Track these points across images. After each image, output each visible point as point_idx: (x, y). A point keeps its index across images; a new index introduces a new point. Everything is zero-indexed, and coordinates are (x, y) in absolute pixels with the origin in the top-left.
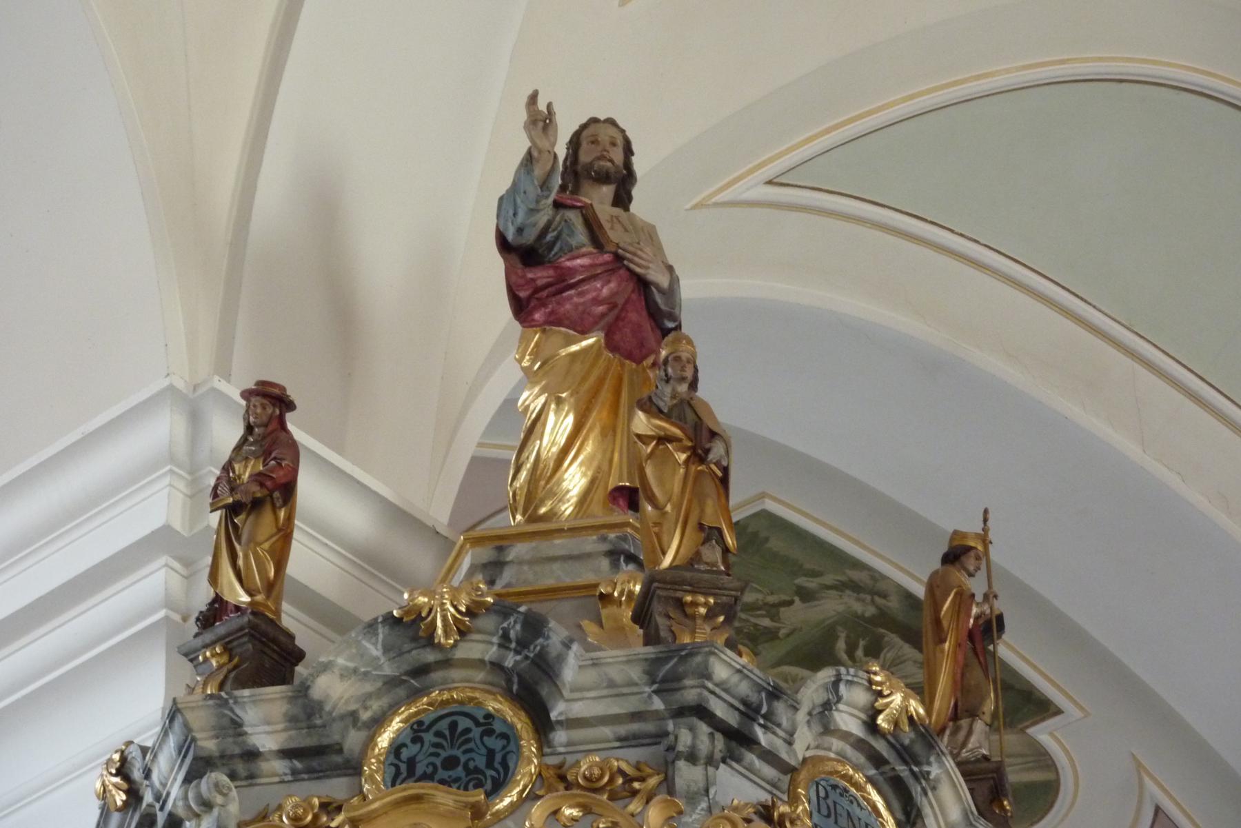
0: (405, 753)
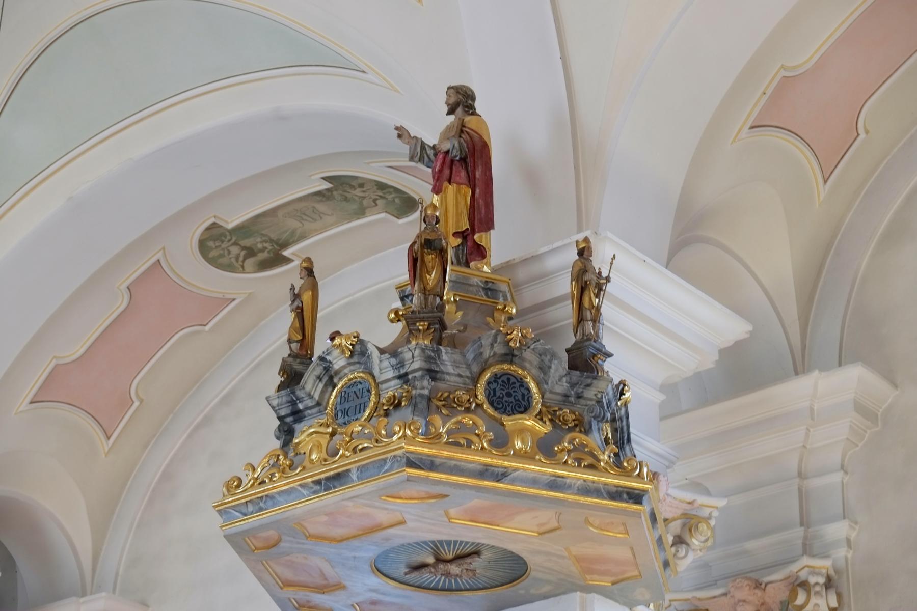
0: (494, 386)
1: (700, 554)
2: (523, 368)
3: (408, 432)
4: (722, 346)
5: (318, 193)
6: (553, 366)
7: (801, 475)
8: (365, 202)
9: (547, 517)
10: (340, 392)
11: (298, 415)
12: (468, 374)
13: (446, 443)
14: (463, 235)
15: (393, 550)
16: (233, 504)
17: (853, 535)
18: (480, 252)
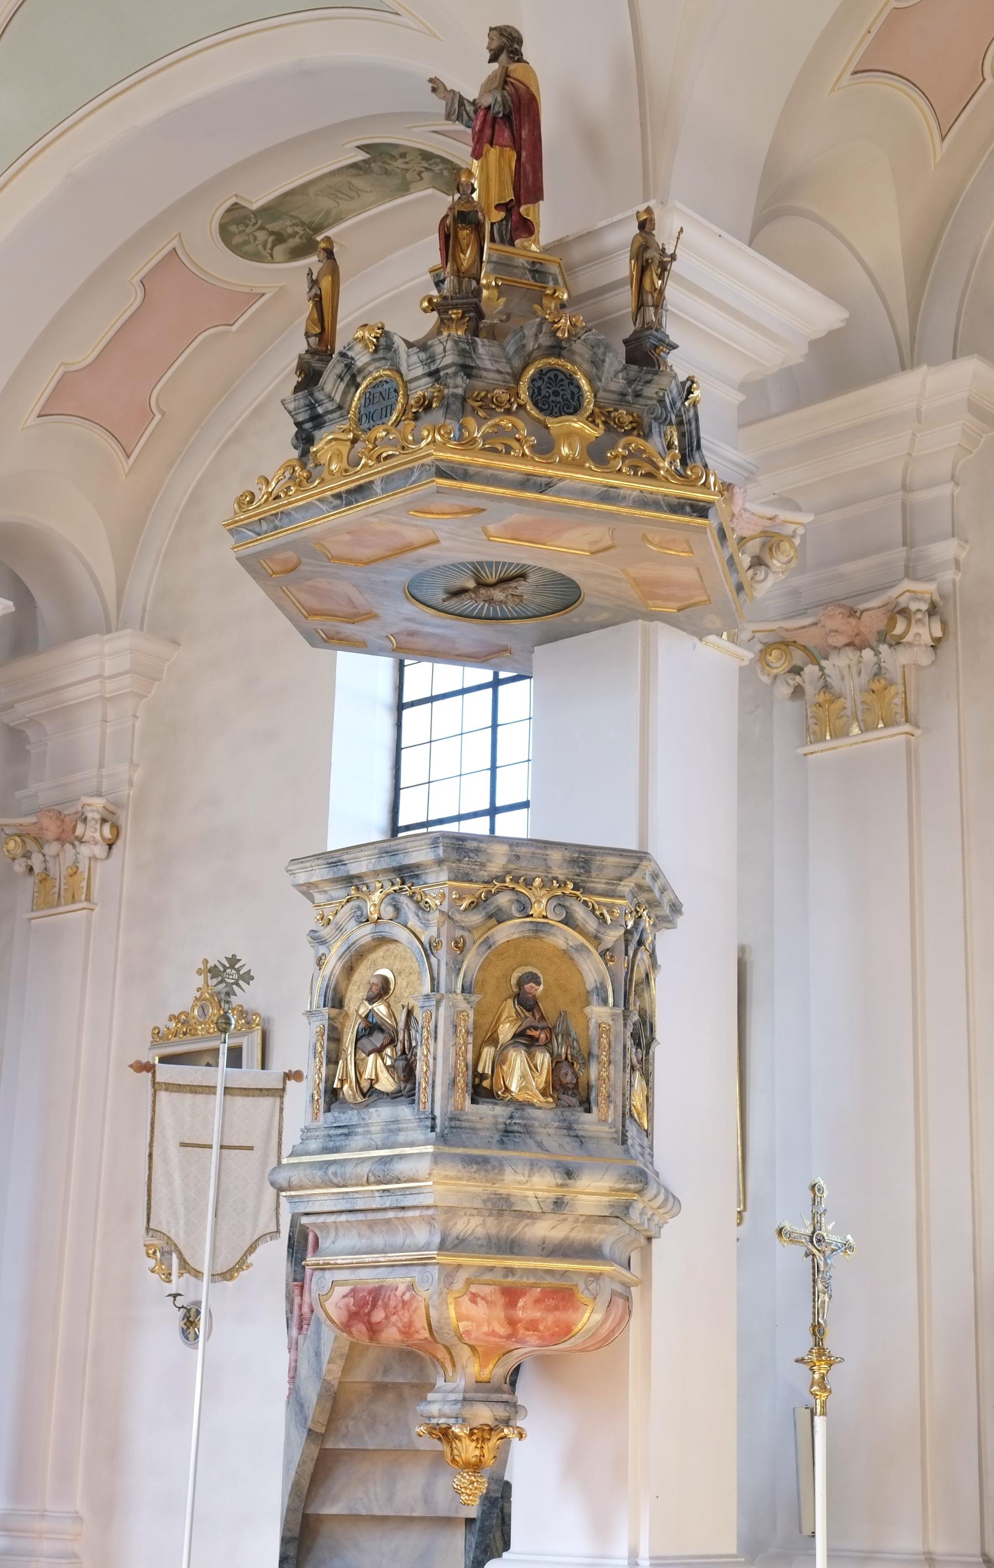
1: (782, 576)
2: (573, 363)
3: (438, 437)
4: (813, 338)
5: (354, 166)
6: (607, 360)
7: (905, 487)
8: (409, 176)
9: (599, 534)
10: (364, 393)
11: (317, 421)
12: (509, 370)
13: (483, 449)
14: (508, 208)
15: (427, 573)
16: (246, 522)
17: (963, 556)
18: (527, 228)
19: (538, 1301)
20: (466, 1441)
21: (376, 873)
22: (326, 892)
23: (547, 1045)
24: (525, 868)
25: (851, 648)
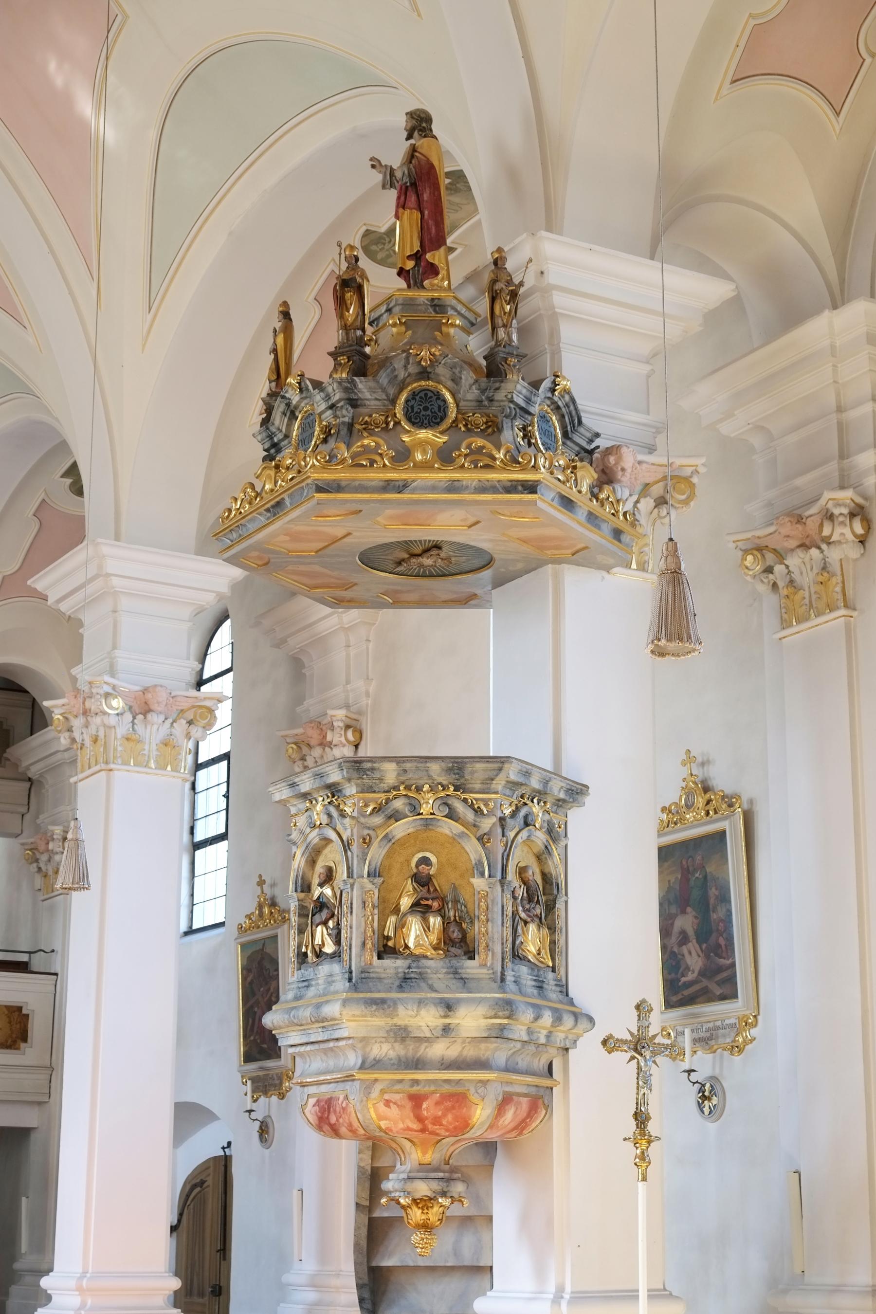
0: (410, 404)
6: (463, 377)
7: (840, 409)
14: (417, 257)
19: (437, 1103)
20: (414, 1208)
21: (318, 790)
22: (295, 805)
23: (441, 912)
24: (413, 777)
25: (801, 548)
